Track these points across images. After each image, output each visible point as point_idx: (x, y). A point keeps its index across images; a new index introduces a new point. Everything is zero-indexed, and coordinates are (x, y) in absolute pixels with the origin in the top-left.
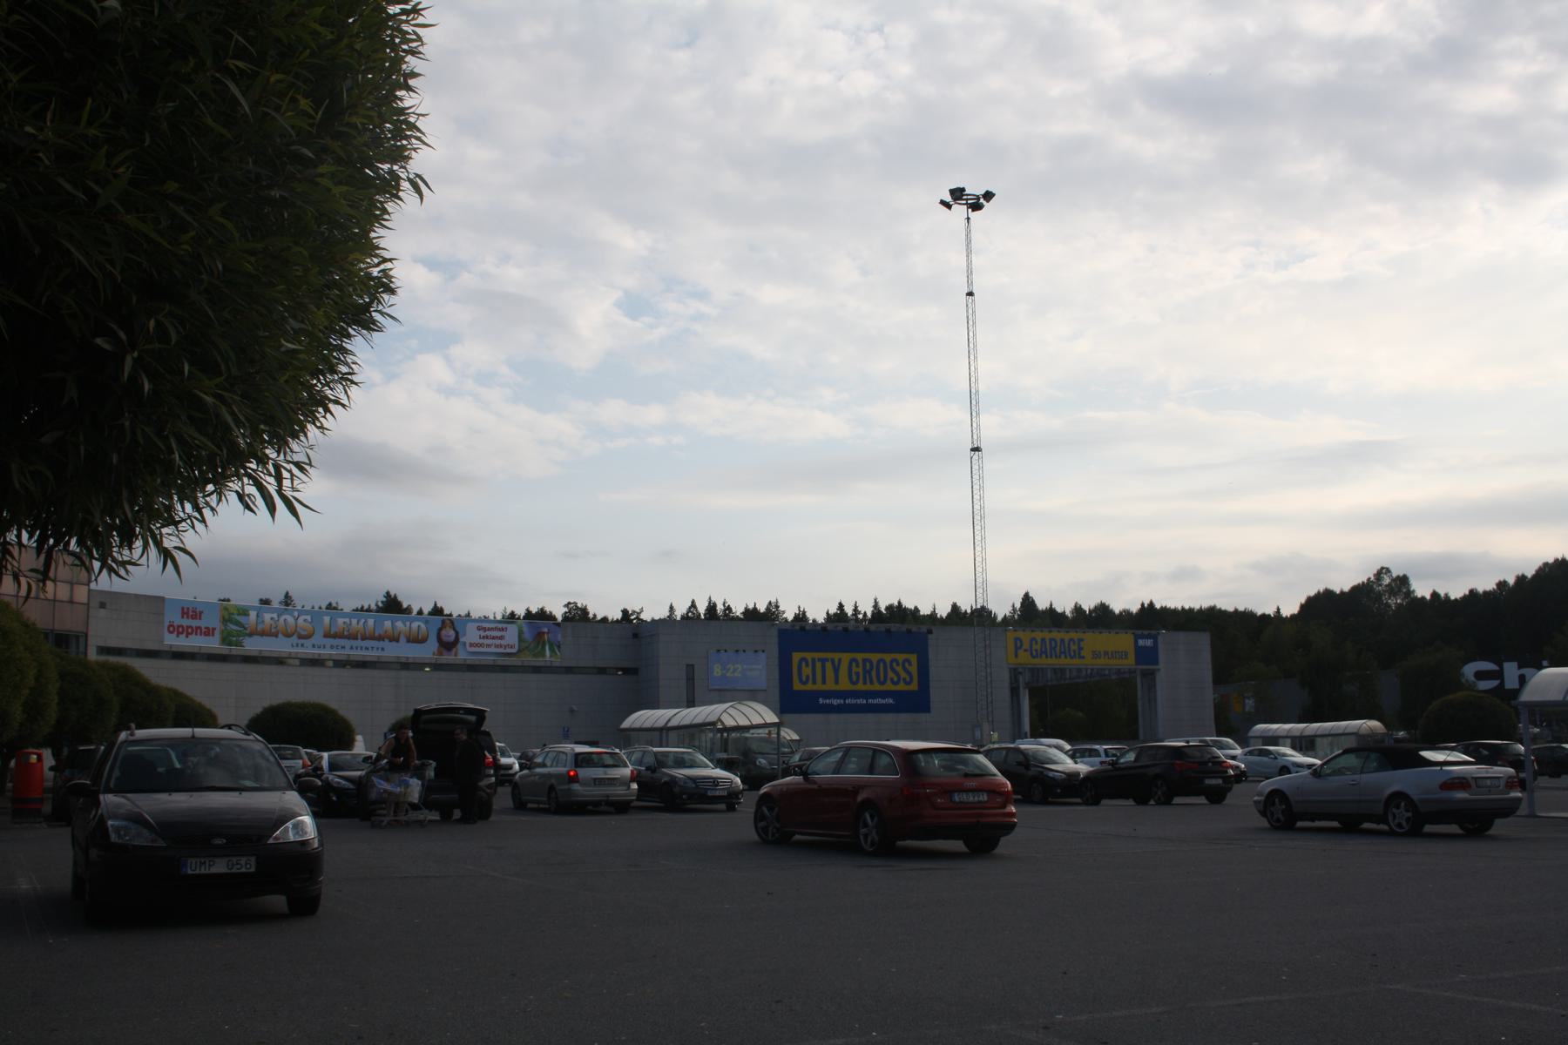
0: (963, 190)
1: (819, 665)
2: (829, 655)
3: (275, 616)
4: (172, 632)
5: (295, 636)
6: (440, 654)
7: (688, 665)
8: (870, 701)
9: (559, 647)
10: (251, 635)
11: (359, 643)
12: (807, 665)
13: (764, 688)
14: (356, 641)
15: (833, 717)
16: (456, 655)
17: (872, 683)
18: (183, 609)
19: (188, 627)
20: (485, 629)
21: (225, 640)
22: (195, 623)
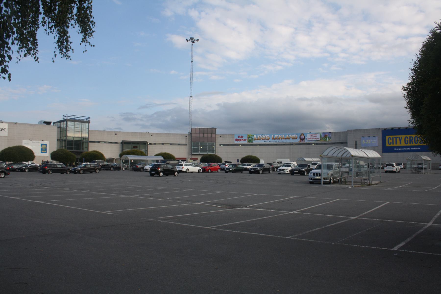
0: (193, 38)
1: (394, 139)
3: (260, 136)
4: (236, 141)
5: (265, 140)
6: (300, 141)
7: (355, 141)
8: (412, 149)
9: (331, 138)
10: (254, 140)
11: (281, 140)
12: (391, 139)
13: (377, 146)
14: (279, 140)
15: (399, 154)
16: (304, 141)
17: (412, 143)
18: (239, 136)
19: (240, 140)
20: (312, 135)
21: (249, 141)
22: (241, 139)
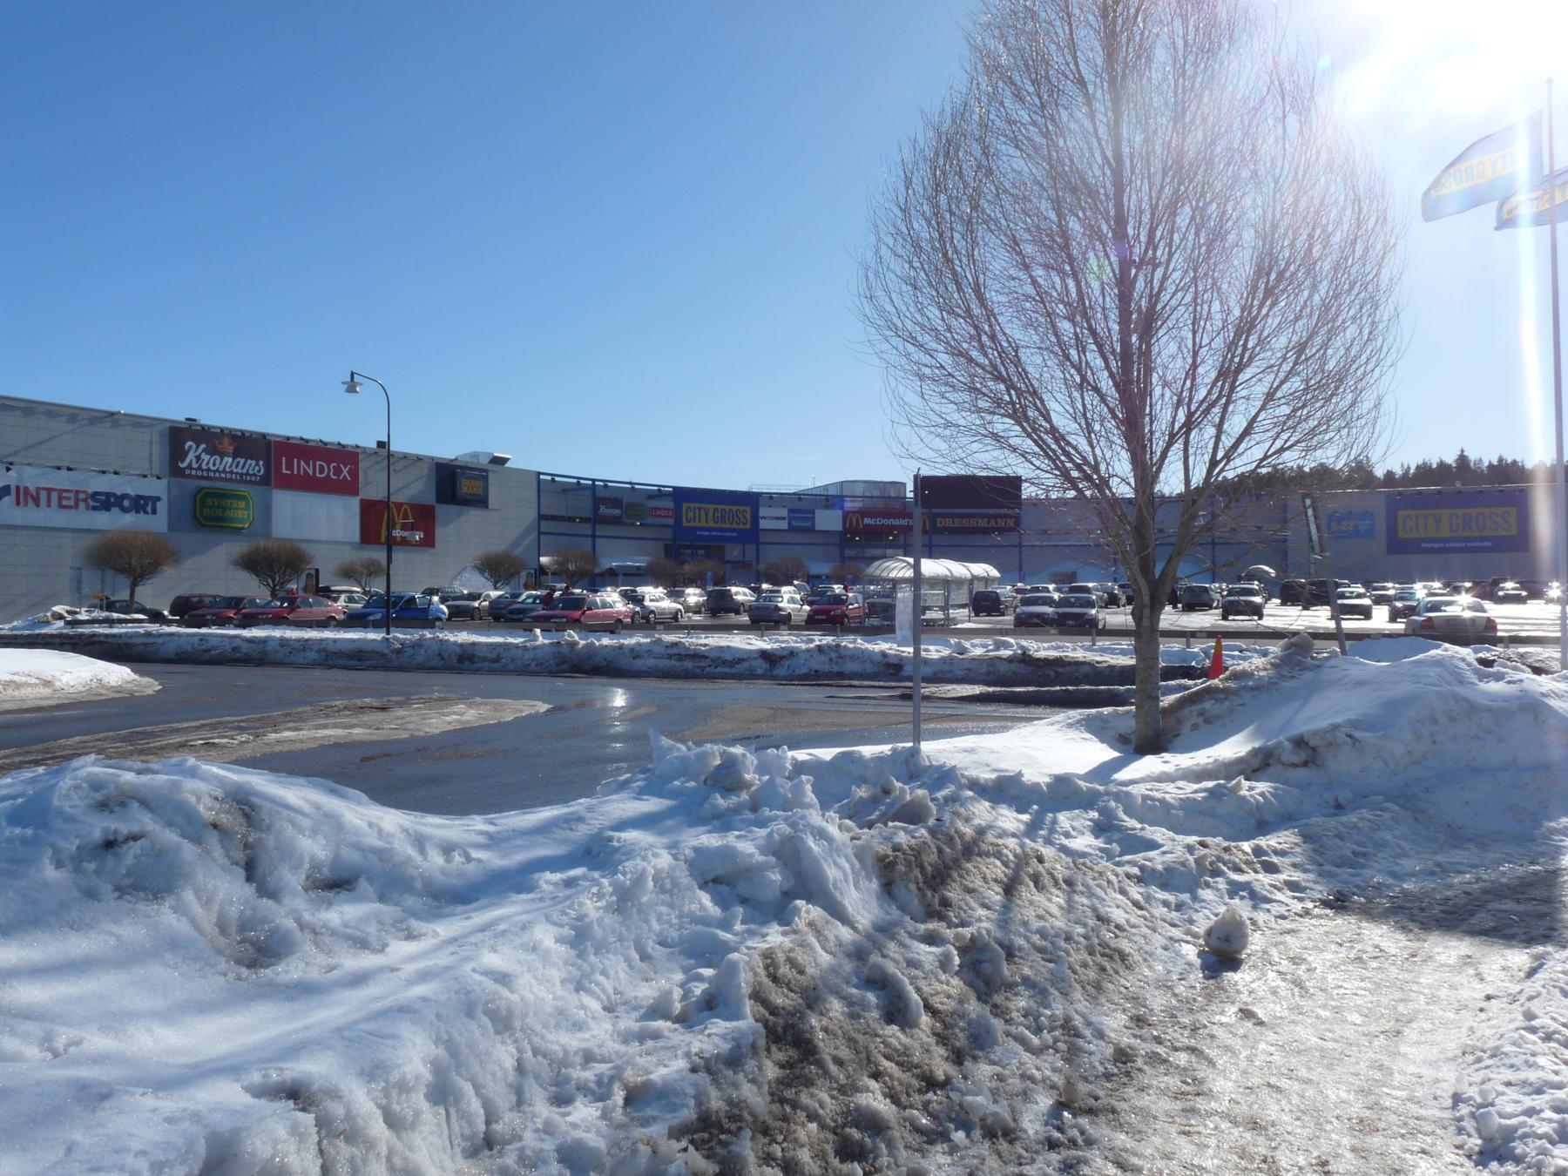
2: (1430, 512)
